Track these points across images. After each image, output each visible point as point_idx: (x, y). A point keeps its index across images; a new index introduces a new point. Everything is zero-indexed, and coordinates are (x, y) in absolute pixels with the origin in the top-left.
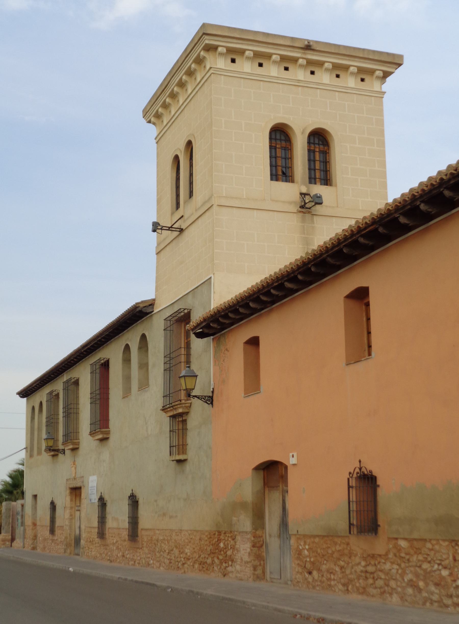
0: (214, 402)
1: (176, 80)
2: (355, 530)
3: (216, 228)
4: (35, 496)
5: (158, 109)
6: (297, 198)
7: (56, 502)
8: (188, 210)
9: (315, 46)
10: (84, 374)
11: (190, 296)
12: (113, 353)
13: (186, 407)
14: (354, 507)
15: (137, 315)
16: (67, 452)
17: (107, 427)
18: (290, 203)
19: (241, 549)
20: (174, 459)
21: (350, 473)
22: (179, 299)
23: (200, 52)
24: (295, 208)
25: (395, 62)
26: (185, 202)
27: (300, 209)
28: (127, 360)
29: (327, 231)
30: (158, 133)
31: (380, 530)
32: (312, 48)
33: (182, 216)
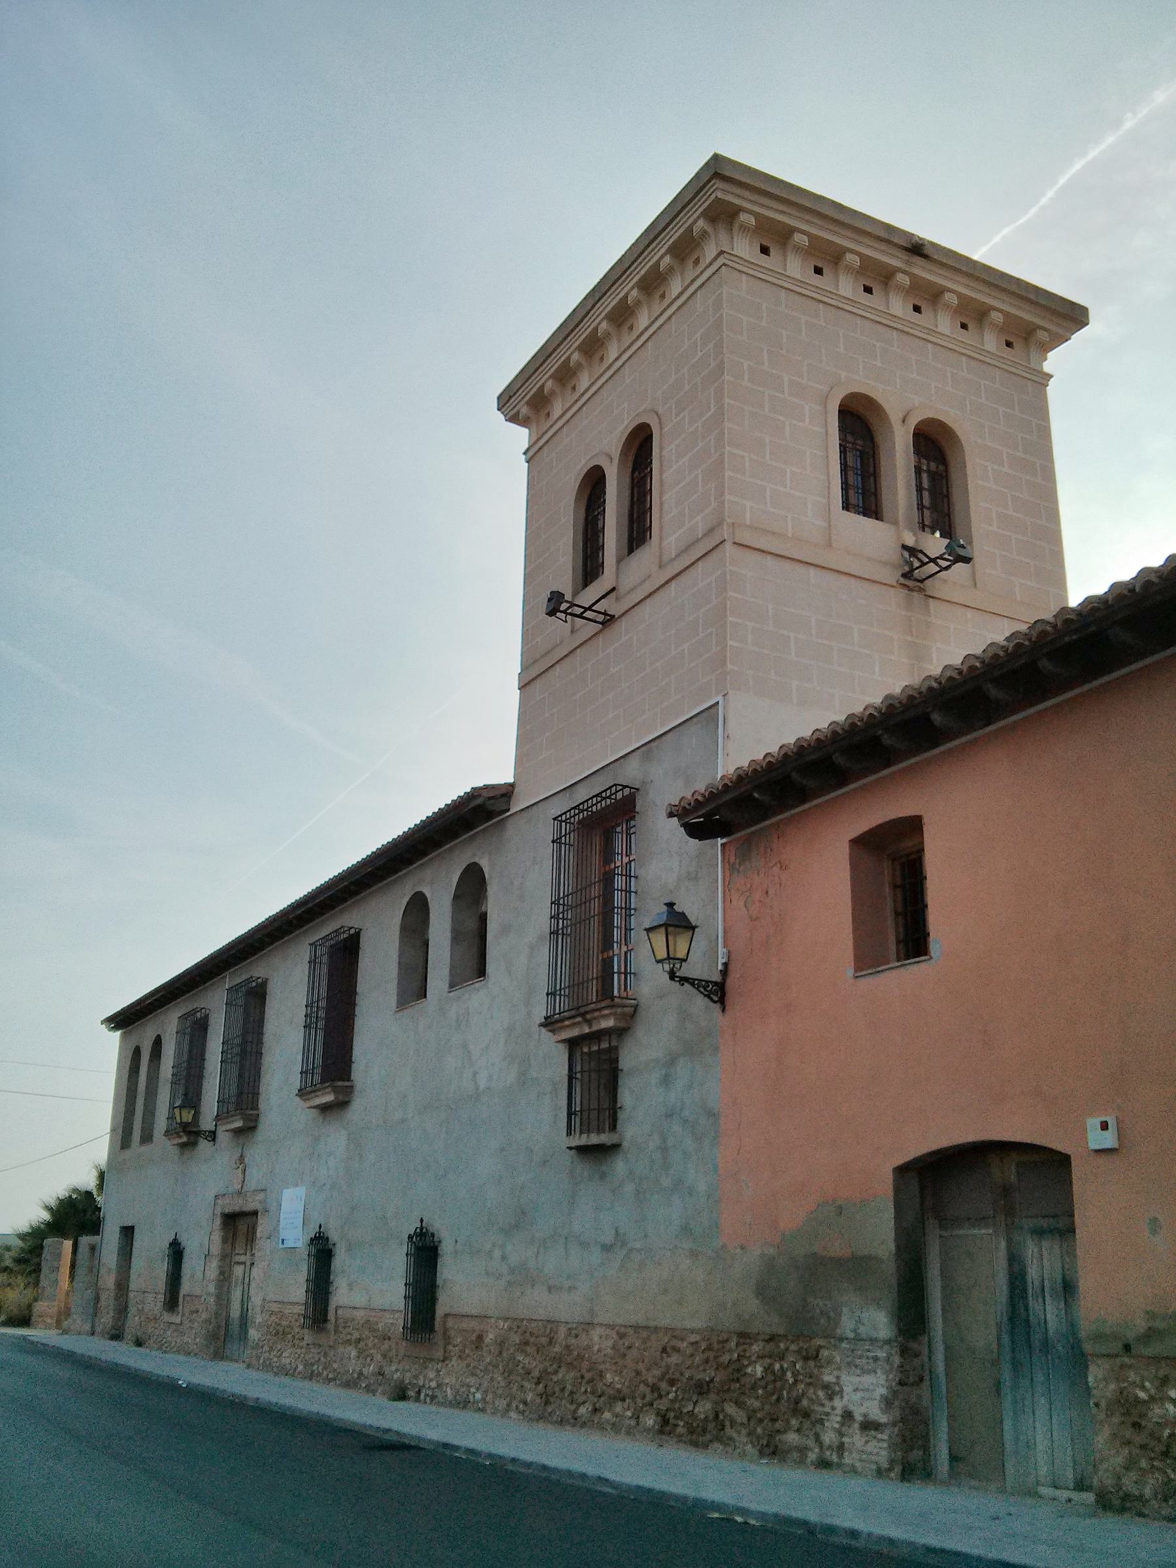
0: (729, 1000)
1: (610, 303)
3: (731, 593)
4: (128, 1232)
6: (893, 554)
7: (184, 1241)
9: (928, 250)
10: (215, 1003)
13: (624, 1015)
15: (475, 815)
16: (223, 1137)
17: (348, 1078)
18: (885, 564)
19: (847, 1389)
20: (574, 1144)
22: (670, 730)
23: (696, 221)
24: (893, 577)
25: (1072, 316)
26: (619, 560)
27: (902, 580)
30: (535, 439)
32: (926, 252)
33: (613, 589)
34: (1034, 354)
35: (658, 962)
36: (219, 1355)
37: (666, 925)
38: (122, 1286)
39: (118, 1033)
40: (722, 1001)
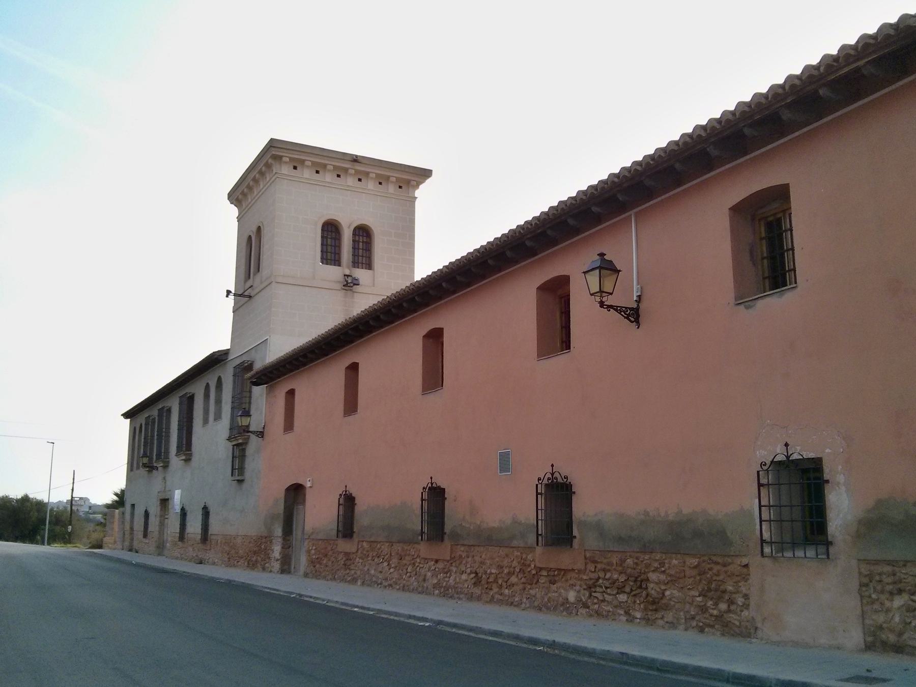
1: (251, 176)
2: (340, 535)
4: (133, 506)
5: (238, 195)
7: (209, 505)
8: (256, 281)
11: (253, 351)
12: (197, 389)
14: (426, 517)
15: (214, 361)
21: (539, 479)
24: (339, 286)
25: (425, 174)
28: (207, 396)
29: (364, 302)
31: (355, 536)
34: (411, 190)
35: (592, 295)
36: (160, 554)
37: (600, 268)
38: (132, 529)
39: (129, 420)
40: (637, 321)
